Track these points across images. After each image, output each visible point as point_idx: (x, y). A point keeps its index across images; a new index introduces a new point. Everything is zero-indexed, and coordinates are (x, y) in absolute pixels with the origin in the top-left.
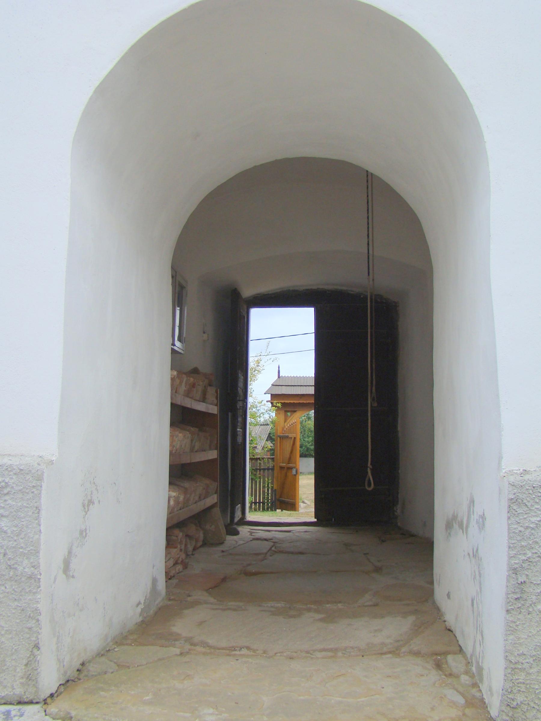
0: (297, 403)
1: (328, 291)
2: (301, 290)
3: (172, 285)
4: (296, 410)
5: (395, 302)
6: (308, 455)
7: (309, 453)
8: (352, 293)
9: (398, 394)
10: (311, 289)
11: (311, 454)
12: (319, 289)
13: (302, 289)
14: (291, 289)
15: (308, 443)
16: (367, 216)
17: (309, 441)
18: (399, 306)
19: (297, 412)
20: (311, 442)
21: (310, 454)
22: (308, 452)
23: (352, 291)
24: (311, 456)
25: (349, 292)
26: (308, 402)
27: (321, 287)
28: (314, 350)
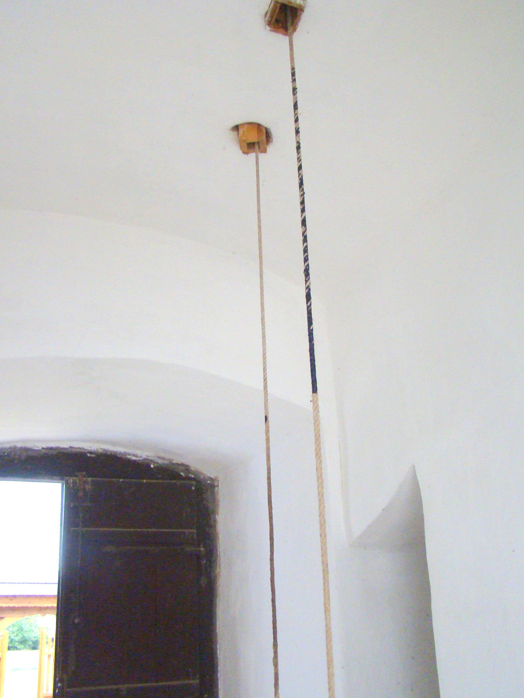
0: (5, 607)
1: (91, 453)
2: (37, 449)
3: (308, 336)
4: (3, 616)
5: (211, 479)
6: (12, 647)
7: (13, 645)
8: (134, 458)
9: (219, 674)
10: (57, 448)
11: (16, 646)
12: (73, 448)
13: (39, 446)
14: (19, 445)
15: (13, 634)
16: (303, 268)
17: (14, 631)
18: (218, 486)
19: (4, 619)
20: (16, 632)
21: (15, 646)
22: (12, 643)
23: (134, 455)
24: (15, 649)
25: (129, 457)
26: (21, 605)
27: (77, 445)
28: (57, 585)
